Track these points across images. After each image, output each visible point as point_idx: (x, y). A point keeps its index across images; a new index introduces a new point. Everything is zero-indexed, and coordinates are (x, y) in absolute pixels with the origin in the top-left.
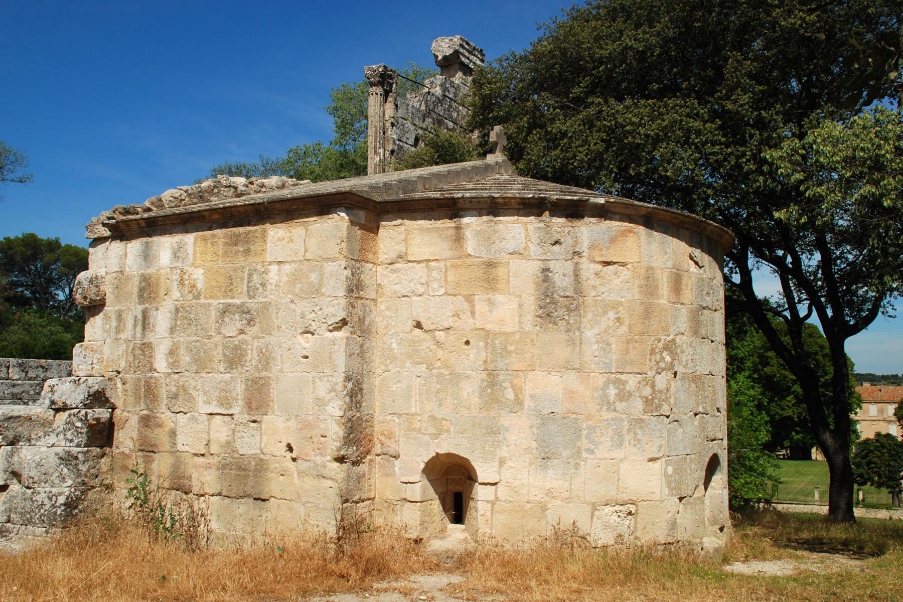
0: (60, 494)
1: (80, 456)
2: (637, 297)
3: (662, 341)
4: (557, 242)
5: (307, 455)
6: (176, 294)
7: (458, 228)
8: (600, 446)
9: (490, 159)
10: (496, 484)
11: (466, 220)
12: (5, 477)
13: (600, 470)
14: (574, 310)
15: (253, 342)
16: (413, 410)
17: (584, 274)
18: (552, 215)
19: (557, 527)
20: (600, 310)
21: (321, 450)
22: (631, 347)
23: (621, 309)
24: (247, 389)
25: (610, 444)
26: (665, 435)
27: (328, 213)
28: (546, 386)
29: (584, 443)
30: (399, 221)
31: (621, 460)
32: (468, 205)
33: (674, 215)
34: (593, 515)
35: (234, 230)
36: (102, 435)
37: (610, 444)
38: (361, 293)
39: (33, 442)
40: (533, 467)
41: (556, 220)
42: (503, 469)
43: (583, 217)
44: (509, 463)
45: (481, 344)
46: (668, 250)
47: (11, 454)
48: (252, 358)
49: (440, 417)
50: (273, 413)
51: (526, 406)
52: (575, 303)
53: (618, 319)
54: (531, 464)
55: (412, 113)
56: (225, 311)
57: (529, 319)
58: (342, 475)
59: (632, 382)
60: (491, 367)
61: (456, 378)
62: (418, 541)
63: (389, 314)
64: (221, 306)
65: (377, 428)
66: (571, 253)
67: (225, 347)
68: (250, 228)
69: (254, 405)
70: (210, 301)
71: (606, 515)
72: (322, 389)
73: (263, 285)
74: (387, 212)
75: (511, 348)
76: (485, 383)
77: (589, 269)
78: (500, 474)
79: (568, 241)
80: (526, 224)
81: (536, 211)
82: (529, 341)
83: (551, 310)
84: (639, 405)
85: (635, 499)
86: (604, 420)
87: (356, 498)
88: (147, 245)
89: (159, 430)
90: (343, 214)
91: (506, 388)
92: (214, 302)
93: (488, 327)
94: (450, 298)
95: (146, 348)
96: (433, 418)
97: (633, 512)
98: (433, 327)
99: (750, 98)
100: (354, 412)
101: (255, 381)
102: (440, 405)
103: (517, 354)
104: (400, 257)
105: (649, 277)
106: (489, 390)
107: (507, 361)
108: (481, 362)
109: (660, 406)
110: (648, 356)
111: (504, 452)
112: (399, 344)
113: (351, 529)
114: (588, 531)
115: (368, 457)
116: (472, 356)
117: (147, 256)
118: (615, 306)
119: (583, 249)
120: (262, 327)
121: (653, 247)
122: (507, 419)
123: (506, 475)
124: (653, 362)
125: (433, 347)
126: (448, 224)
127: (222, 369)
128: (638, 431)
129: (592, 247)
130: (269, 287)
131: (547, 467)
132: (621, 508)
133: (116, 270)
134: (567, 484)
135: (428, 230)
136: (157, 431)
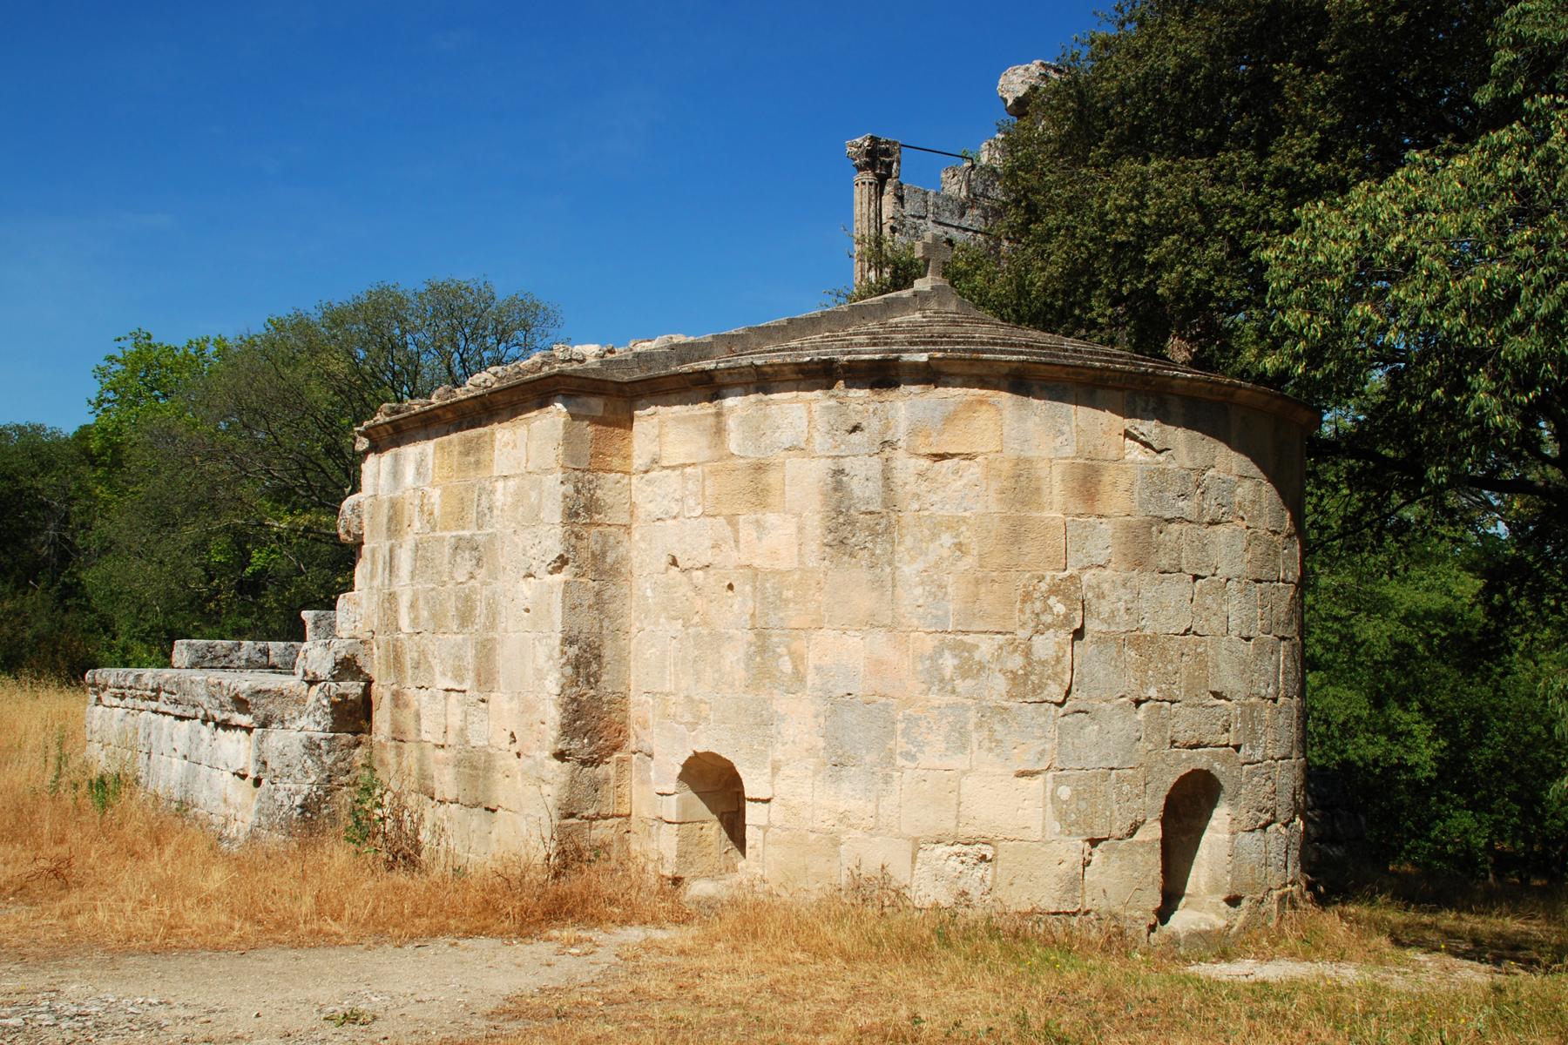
0: (298, 793)
1: (323, 744)
2: (994, 508)
3: (1048, 579)
4: (855, 428)
6: (417, 525)
7: (719, 415)
8: (926, 749)
9: (921, 285)
10: (768, 801)
11: (729, 402)
13: (927, 786)
16: (667, 688)
17: (899, 476)
18: (848, 386)
19: (856, 872)
22: (983, 590)
23: (963, 528)
24: (476, 656)
25: (944, 745)
26: (1053, 733)
27: (547, 405)
28: (841, 652)
29: (901, 743)
30: (652, 409)
31: (964, 773)
32: (728, 380)
34: (914, 859)
35: (467, 433)
36: (353, 716)
37: (944, 745)
38: (597, 517)
44: (785, 771)
45: (748, 588)
46: (1066, 428)
47: (261, 740)
51: (809, 684)
52: (884, 521)
53: (959, 546)
54: (816, 773)
55: (936, 205)
58: (565, 778)
59: (986, 647)
60: (760, 623)
62: (677, 881)
65: (634, 712)
67: (458, 597)
68: (481, 430)
71: (938, 859)
73: (490, 509)
74: (641, 396)
75: (788, 594)
77: (907, 467)
79: (873, 425)
80: (810, 402)
82: (813, 583)
84: (1000, 684)
85: (991, 835)
86: (933, 708)
87: (591, 812)
88: (396, 458)
90: (559, 406)
92: (447, 534)
93: (757, 563)
94: (709, 520)
95: (392, 597)
96: (689, 699)
97: (989, 856)
98: (689, 564)
99: (1314, 140)
100: (584, 689)
104: (655, 461)
109: (1042, 686)
111: (778, 753)
112: (653, 590)
113: (570, 856)
115: (616, 755)
116: (736, 607)
118: (952, 524)
121: (1030, 424)
122: (782, 704)
123: (782, 788)
124: (1028, 614)
125: (691, 594)
126: (706, 408)
128: (997, 727)
129: (913, 432)
132: (966, 849)
134: (871, 806)
135: (684, 420)
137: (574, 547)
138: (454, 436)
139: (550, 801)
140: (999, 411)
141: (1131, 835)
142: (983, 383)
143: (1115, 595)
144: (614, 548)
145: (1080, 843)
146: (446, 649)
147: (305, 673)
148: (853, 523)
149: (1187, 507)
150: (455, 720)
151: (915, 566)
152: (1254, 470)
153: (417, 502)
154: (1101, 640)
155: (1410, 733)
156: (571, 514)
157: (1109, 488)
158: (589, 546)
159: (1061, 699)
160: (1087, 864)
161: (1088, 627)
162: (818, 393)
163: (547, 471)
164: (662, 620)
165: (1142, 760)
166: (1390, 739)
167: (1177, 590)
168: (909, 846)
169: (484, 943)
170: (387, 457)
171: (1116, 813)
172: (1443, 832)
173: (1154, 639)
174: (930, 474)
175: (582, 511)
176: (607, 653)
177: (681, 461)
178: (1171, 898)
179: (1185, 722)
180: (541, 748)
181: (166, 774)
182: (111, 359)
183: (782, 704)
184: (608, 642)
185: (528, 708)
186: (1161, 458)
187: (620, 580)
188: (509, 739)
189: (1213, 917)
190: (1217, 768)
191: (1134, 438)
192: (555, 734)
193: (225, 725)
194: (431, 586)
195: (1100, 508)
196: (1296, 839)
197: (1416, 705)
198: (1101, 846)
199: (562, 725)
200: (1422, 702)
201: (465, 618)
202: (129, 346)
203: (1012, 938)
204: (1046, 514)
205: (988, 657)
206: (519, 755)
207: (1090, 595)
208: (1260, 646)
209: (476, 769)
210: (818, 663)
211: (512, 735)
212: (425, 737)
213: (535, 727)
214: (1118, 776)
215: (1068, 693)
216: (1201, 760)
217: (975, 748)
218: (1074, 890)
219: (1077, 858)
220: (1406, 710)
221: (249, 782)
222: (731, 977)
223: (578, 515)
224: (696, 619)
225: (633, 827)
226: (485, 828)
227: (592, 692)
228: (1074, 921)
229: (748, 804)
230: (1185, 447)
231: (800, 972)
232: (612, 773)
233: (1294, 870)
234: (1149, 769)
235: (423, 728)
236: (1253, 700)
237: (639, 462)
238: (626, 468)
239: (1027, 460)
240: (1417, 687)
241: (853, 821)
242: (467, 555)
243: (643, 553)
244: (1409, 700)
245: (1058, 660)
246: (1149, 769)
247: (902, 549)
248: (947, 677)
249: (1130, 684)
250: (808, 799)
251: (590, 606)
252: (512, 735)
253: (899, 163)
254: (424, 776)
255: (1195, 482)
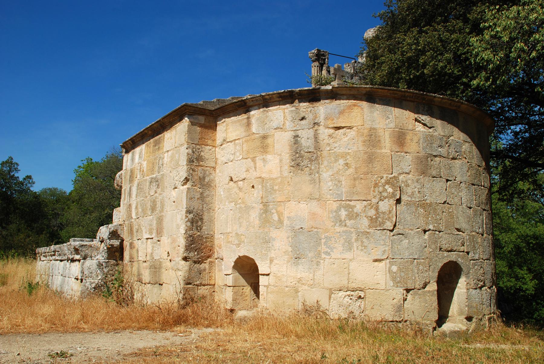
2: (361, 148)
3: (385, 178)
4: (303, 119)
6: (139, 176)
7: (248, 118)
8: (334, 250)
10: (268, 275)
11: (252, 113)
13: (335, 266)
14: (314, 160)
16: (229, 230)
17: (321, 137)
18: (300, 102)
20: (333, 159)
23: (348, 157)
24: (157, 223)
25: (342, 248)
26: (389, 243)
29: (323, 248)
30: (224, 120)
32: (251, 104)
33: (391, 92)
35: (156, 138)
36: (116, 253)
37: (342, 248)
38: (201, 163)
39: (93, 258)
40: (289, 264)
41: (301, 104)
42: (272, 265)
43: (320, 100)
44: (275, 261)
45: (260, 186)
46: (390, 116)
49: (240, 233)
51: (285, 225)
52: (315, 155)
53: (347, 164)
54: (288, 262)
57: (286, 168)
58: (187, 268)
59: (359, 207)
60: (265, 200)
61: (248, 208)
62: (232, 311)
65: (216, 242)
66: (312, 124)
68: (160, 136)
73: (162, 165)
75: (276, 188)
76: (262, 211)
77: (324, 132)
80: (284, 109)
81: (290, 101)
82: (286, 182)
83: (299, 161)
84: (365, 222)
85: (363, 287)
86: (337, 232)
87: (198, 282)
90: (186, 118)
91: (273, 213)
92: (148, 178)
93: (263, 176)
94: (244, 160)
95: (130, 205)
97: (362, 296)
98: (237, 179)
100: (195, 232)
102: (240, 227)
103: (279, 191)
104: (224, 140)
105: (371, 135)
106: (264, 215)
107: (273, 196)
108: (260, 198)
109: (383, 223)
110: (372, 189)
111: (272, 254)
114: (327, 308)
115: (209, 260)
116: (255, 195)
118: (344, 156)
119: (320, 120)
121: (375, 114)
122: (274, 233)
123: (274, 269)
126: (244, 116)
128: (365, 240)
129: (326, 119)
131: (298, 264)
132: (352, 293)
134: (311, 275)
137: (192, 175)
138: (152, 140)
139: (180, 278)
140: (362, 109)
141: (424, 287)
142: (355, 98)
143: (413, 186)
144: (208, 176)
145: (401, 291)
146: (146, 223)
147: (100, 238)
148: (302, 157)
149: (443, 151)
150: (149, 250)
151: (328, 173)
152: (469, 140)
153: (139, 168)
154: (408, 204)
155: (523, 278)
156: (190, 161)
157: (409, 141)
158: (198, 176)
159: (391, 228)
160: (405, 300)
161: (403, 198)
162: (288, 105)
163: (182, 145)
164: (227, 203)
165: (427, 256)
166: (516, 280)
167: (439, 185)
168: (328, 292)
169: (145, 332)
170: (130, 154)
171: (417, 278)
172: (538, 316)
173: (431, 205)
174: (334, 135)
175: (195, 160)
176: (205, 218)
177: (234, 138)
178: (442, 318)
179: (445, 241)
180: (178, 257)
181: (57, 282)
182: (80, 167)
184: (206, 214)
185: (174, 241)
186: (431, 130)
187: (211, 189)
188: (167, 255)
189: (460, 325)
190: (460, 261)
191: (419, 122)
192: (183, 250)
193: (73, 260)
194: (142, 199)
195: (406, 149)
196: (494, 294)
197: (525, 268)
198: (411, 292)
199: (186, 246)
200: (528, 267)
201: (153, 209)
202: (85, 163)
203: (373, 330)
204: (383, 151)
205: (360, 211)
206: (170, 261)
207: (403, 185)
208: (475, 211)
209: (156, 268)
210: (288, 215)
211: (168, 253)
212: (140, 259)
213: (176, 248)
214: (417, 262)
215: (395, 226)
216: (453, 257)
217: (355, 249)
218: (400, 311)
219: (400, 297)
220: (522, 270)
221: (79, 281)
222: (243, 341)
223: (193, 162)
224: (240, 201)
225: (216, 290)
226: (159, 292)
227: (199, 233)
228: (400, 325)
229: (260, 276)
230: (441, 127)
231: (277, 341)
232: (207, 267)
233: (493, 308)
234: (431, 260)
235: (139, 255)
236: (473, 233)
237: (218, 142)
238: (214, 145)
239: (374, 129)
240: (525, 262)
241: (304, 282)
242: (154, 184)
243: (220, 178)
244: (522, 267)
245: (390, 212)
246: (431, 260)
247: (323, 166)
248: (343, 219)
249: (421, 223)
250: (285, 273)
251: (198, 198)
252: (168, 253)
253: (328, 59)
254: (139, 274)
255: (445, 141)
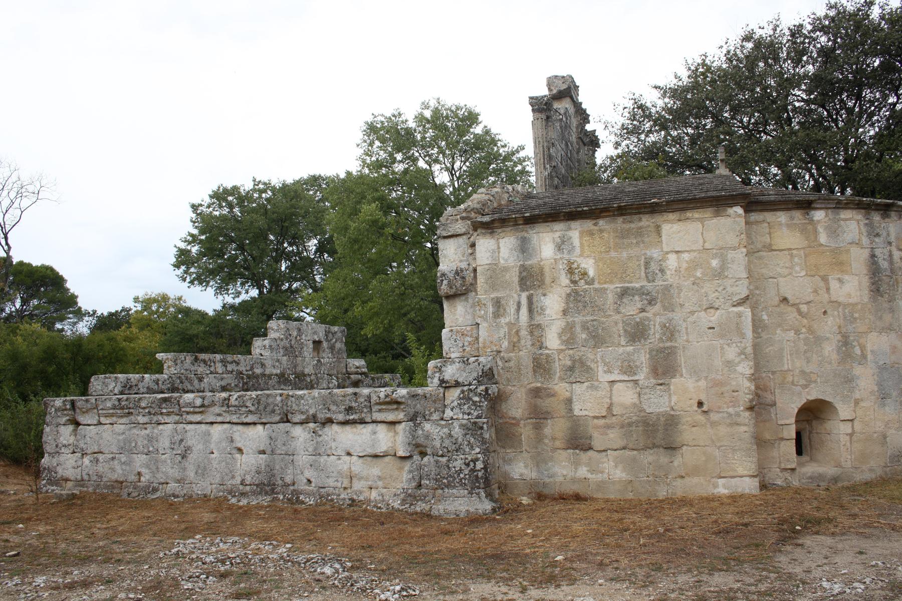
5: (720, 408)
10: (852, 420)
12: (409, 449)
15: (656, 317)
16: (786, 367)
21: (734, 403)
42: (857, 409)
44: (862, 404)
48: (655, 334)
50: (682, 376)
56: (624, 293)
60: (844, 330)
63: (757, 292)
64: (619, 290)
69: (660, 371)
70: (606, 286)
72: (731, 353)
75: (856, 315)
78: (855, 411)
89: (552, 399)
92: (612, 287)
94: (809, 278)
96: (803, 372)
101: (661, 350)
111: (857, 395)
112: (769, 316)
117: (524, 248)
120: (664, 306)
122: (858, 370)
127: (623, 343)
130: (668, 272)
131: (884, 405)
133: (488, 262)
136: (548, 401)
183: (858, 370)
